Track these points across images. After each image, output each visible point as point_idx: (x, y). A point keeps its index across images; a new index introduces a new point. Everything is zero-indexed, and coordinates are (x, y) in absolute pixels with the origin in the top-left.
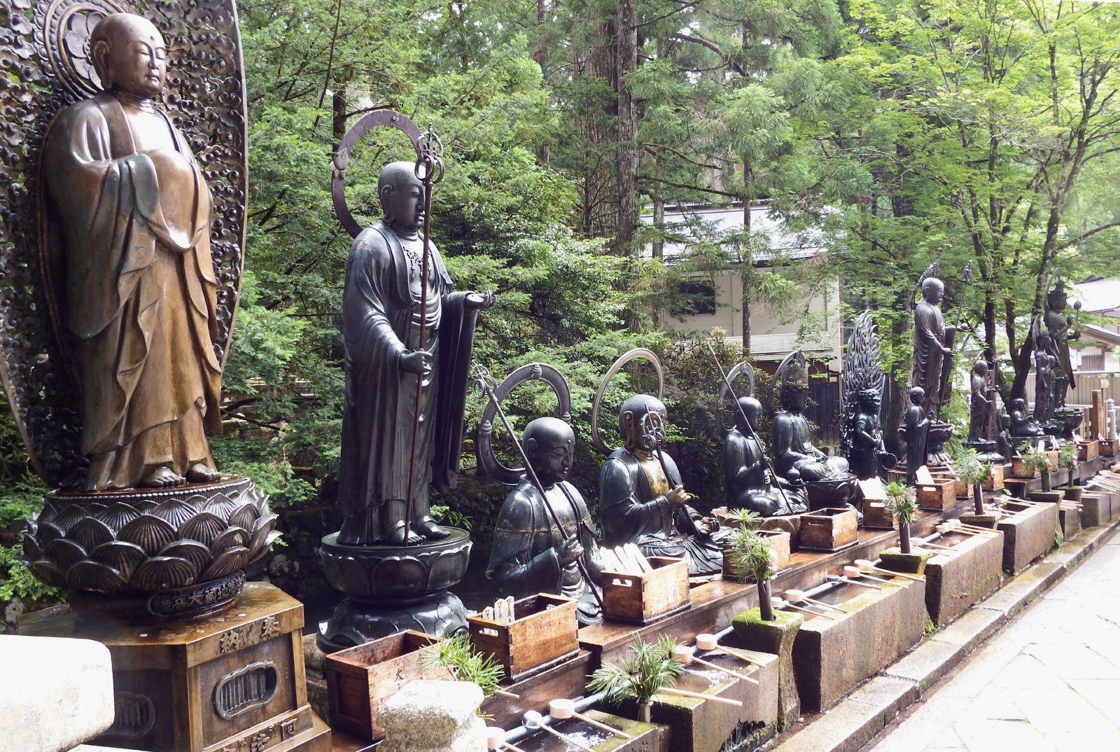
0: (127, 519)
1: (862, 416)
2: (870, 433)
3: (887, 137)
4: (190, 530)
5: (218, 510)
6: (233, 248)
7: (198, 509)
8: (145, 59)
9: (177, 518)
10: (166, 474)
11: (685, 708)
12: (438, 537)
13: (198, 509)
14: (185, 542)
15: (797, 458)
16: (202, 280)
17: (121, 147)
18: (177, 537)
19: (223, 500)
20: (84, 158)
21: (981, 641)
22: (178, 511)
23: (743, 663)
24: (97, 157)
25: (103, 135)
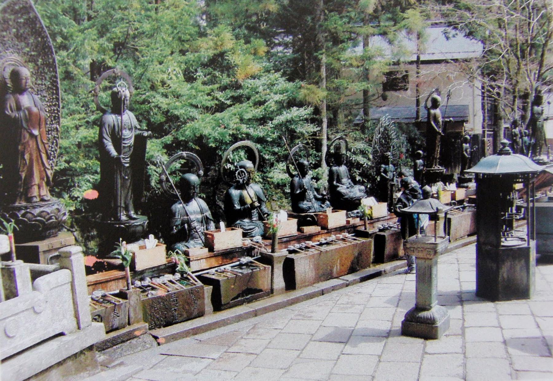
0: (23, 212)
1: (383, 166)
2: (386, 174)
3: (257, 90)
4: (40, 215)
5: (48, 210)
6: (56, 127)
7: (42, 209)
8: (24, 81)
9: (37, 211)
10: (35, 200)
11: (511, 300)
12: (135, 219)
13: (42, 209)
14: (39, 218)
15: (338, 186)
16: (43, 143)
17: (19, 108)
18: (36, 217)
19: (49, 206)
20: (8, 112)
21: (334, 288)
22: (36, 209)
23: (196, 281)
24: (12, 111)
25: (14, 105)
